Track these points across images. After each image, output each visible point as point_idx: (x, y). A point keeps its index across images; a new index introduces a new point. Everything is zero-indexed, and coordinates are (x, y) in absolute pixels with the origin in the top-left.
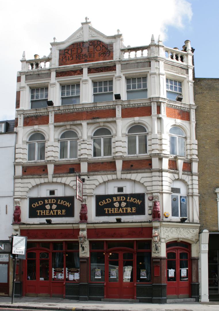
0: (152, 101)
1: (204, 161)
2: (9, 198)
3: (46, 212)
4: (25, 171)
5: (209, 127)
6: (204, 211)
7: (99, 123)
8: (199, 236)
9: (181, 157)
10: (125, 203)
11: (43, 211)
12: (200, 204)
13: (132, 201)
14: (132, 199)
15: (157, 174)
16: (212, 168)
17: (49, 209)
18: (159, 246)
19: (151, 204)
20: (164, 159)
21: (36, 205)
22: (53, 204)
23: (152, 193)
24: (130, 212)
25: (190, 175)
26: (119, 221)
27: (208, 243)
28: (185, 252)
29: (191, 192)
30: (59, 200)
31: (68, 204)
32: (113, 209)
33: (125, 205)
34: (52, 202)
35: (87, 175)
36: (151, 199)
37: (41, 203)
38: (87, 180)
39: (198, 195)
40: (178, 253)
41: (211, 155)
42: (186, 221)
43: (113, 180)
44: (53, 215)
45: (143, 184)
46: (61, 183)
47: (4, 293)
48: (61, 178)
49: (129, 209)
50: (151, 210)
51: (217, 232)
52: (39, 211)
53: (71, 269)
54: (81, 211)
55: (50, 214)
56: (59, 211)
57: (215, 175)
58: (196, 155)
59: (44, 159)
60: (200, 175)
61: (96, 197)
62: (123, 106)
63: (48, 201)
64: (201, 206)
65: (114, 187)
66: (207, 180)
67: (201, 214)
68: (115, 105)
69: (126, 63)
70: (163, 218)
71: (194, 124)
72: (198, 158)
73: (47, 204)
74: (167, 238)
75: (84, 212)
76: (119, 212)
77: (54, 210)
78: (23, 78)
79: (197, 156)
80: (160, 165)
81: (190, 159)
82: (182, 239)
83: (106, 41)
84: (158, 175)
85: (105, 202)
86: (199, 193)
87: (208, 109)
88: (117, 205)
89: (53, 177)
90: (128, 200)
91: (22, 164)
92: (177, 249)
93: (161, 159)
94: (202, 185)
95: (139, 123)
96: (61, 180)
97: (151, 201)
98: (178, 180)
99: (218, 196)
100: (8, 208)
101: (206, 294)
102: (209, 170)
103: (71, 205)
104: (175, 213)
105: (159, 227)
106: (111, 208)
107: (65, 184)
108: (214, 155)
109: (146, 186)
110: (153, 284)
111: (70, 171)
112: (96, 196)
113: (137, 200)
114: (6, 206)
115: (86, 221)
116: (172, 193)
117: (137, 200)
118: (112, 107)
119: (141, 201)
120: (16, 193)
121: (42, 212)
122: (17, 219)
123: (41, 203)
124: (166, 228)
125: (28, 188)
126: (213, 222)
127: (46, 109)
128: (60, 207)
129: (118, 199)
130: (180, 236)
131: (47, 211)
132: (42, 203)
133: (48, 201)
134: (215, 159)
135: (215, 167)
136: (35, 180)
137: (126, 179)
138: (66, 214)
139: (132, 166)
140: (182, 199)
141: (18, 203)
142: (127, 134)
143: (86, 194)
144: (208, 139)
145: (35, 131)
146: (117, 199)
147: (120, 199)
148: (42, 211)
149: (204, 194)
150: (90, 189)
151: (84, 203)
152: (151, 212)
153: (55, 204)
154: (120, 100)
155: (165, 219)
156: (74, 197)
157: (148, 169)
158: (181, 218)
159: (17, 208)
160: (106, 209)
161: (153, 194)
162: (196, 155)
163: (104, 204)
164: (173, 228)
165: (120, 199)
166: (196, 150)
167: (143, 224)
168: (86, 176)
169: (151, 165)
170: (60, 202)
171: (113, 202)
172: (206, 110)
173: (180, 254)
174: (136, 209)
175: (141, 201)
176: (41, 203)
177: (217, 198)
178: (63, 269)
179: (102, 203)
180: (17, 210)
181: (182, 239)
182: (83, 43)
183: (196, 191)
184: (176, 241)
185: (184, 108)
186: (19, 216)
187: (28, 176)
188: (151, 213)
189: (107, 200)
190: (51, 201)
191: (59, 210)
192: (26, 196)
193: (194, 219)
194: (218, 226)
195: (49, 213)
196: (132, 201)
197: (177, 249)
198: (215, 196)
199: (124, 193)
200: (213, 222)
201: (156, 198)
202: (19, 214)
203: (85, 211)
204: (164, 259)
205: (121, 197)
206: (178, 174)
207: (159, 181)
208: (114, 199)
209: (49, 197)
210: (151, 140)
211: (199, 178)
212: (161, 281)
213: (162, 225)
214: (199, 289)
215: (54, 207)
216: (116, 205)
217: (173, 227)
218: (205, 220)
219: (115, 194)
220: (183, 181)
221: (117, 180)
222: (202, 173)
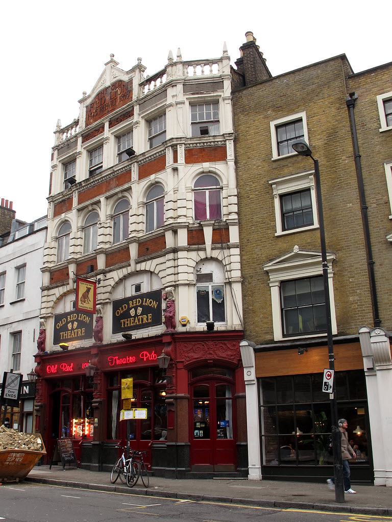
0: (166, 146)
5: (255, 163)
6: (251, 307)
7: (116, 194)
15: (171, 256)
20: (179, 231)
35: (104, 274)
43: (130, 275)
60: (241, 246)
62: (140, 163)
67: (247, 312)
68: (131, 164)
69: (143, 101)
71: (232, 164)
78: (56, 152)
83: (125, 78)
87: (253, 134)
91: (75, 260)
93: (175, 232)
95: (210, 172)
98: (207, 260)
101: (255, 465)
106: (65, 331)
107: (152, 273)
118: (219, 143)
122: (41, 344)
123: (125, 306)
125: (110, 286)
126: (266, 326)
127: (75, 186)
128: (147, 310)
130: (208, 357)
139: (148, 249)
140: (218, 292)
142: (193, 188)
143: (102, 301)
144: (253, 183)
145: (203, 172)
149: (250, 276)
151: (99, 316)
154: (207, 135)
163: (151, 306)
172: (249, 135)
180: (43, 332)
182: (106, 89)
183: (237, 274)
185: (202, 144)
187: (153, 255)
192: (109, 299)
198: (265, 278)
200: (266, 326)
206: (205, 250)
210: (177, 201)
215: (140, 310)
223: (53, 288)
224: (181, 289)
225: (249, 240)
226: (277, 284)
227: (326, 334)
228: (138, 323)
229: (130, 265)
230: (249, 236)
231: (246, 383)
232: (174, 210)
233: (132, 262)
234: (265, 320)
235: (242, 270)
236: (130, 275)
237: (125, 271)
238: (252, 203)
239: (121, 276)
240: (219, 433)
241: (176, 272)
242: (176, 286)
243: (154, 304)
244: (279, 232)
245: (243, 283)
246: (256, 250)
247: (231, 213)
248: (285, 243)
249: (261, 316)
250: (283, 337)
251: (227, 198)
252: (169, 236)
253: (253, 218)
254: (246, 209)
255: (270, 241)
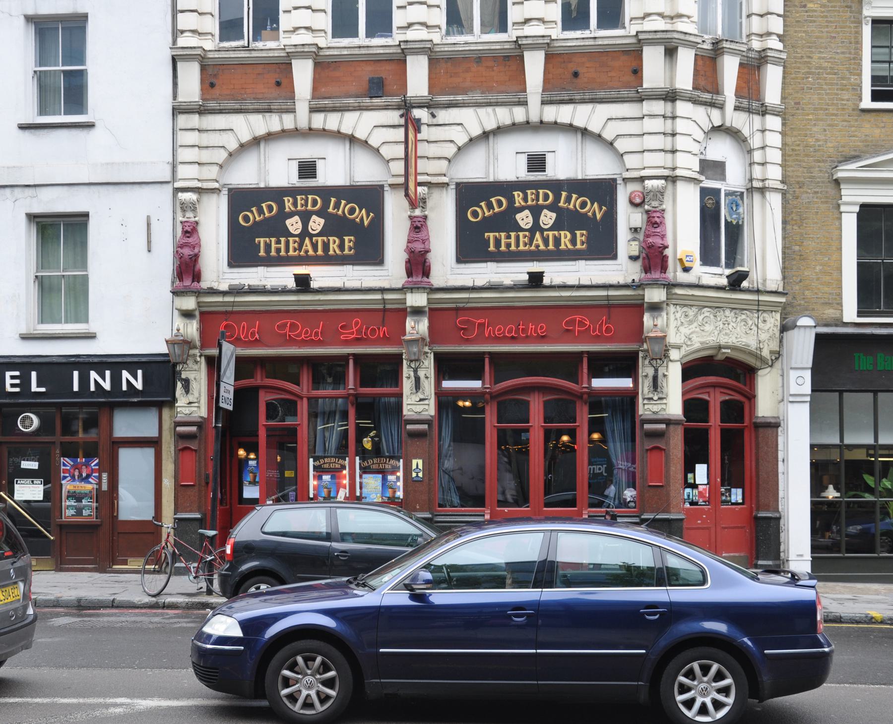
1: (802, 57)
2: (66, 188)
3: (287, 243)
4: (212, 85)
6: (797, 248)
8: (781, 341)
9: (733, 46)
10: (554, 215)
11: (278, 242)
12: (784, 222)
13: (575, 206)
14: (578, 199)
15: (658, 107)
16: (824, 87)
17: (298, 232)
18: (665, 376)
19: (637, 218)
21: (483, 211)
22: (542, 207)
23: (642, 179)
24: (570, 246)
25: (759, 114)
26: (303, 282)
27: (810, 365)
28: (737, 397)
29: (760, 177)
30: (333, 200)
31: (362, 216)
32: (513, 234)
33: (551, 222)
34: (309, 207)
36: (638, 200)
37: (270, 210)
38: (428, 125)
39: (781, 186)
40: (715, 400)
41: (825, 35)
42: (745, 284)
43: (514, 128)
44: (311, 257)
45: (611, 144)
46: (339, 132)
47: (142, 561)
48: (339, 114)
49: (565, 237)
50: (637, 243)
51: (836, 325)
52: (262, 240)
53: (370, 461)
54: (409, 242)
55: (302, 253)
56: (335, 242)
57: (836, 115)
58: (778, 36)
59: (277, 39)
61: (456, 189)
63: (295, 204)
64: (788, 227)
65: (517, 153)
66: (808, 132)
70: (675, 271)
72: (785, 47)
73: (521, 209)
74: (687, 345)
75: (419, 247)
76: (533, 248)
77: (314, 239)
79: (781, 38)
80: (668, 74)
81: (759, 52)
82: (729, 351)
84: (663, 113)
85: (485, 210)
86: (782, 182)
88: (526, 220)
89: (313, 110)
90: (561, 204)
92: (714, 386)
93: (671, 52)
94: (793, 150)
96: (340, 122)
97: (639, 210)
99: (843, 192)
100: (153, 227)
101: (802, 556)
102: (819, 94)
103: (373, 219)
104: (708, 256)
105: (665, 306)
107: (352, 139)
108: (835, 37)
109: (622, 151)
110: (643, 517)
111: (370, 89)
112: (458, 184)
113: (592, 204)
114: (148, 218)
115: (425, 279)
116: (701, 181)
117: (592, 204)
119: (604, 208)
120: (184, 171)
121: (273, 246)
123: (270, 208)
124: (685, 309)
126: (826, 289)
129: (529, 197)
130: (723, 340)
131: (291, 239)
132: (504, 205)
133: (295, 204)
134: (837, 53)
135: (837, 84)
136: (247, 120)
137: (556, 123)
138: (356, 253)
140: (736, 197)
141: (192, 207)
146: (525, 199)
147: (538, 200)
148: (273, 240)
149: (798, 183)
150: (439, 158)
152: (637, 247)
153: (319, 214)
155: (682, 277)
156: (382, 186)
157: (627, 86)
158: (728, 272)
159: (187, 228)
160: (491, 235)
161: (647, 182)
162: (778, 36)
163: (484, 218)
164: (706, 309)
165: (538, 199)
166: (779, 15)
167: (612, 293)
168: (426, 109)
169: (637, 72)
170: (337, 206)
171: (513, 210)
173: (724, 403)
174: (588, 238)
175: (604, 208)
176: (270, 208)
177: (840, 202)
178: (347, 462)
179: (476, 211)
181: (729, 351)
183: (774, 173)
184: (709, 359)
186: (195, 258)
187: (601, 94)
188: (636, 253)
189: (493, 200)
190: (307, 201)
191: (331, 239)
193: (768, 277)
194: (841, 304)
195: (300, 249)
196: (575, 206)
197: (714, 386)
198: (832, 191)
199: (548, 178)
200: (826, 289)
201: (655, 198)
202: (196, 251)
203: (424, 242)
204: (677, 422)
205: (541, 191)
206: (721, 107)
207: (664, 134)
208: (516, 196)
209: (298, 185)
211: (783, 124)
212: (669, 505)
213: (674, 296)
214: (782, 535)
216: (524, 219)
217: (702, 304)
218: (800, 281)
219: (520, 179)
220: (734, 134)
221: (296, 134)
222: (796, 103)
223: (221, 112)
224: (680, 185)
225: (798, 103)
226: (857, 209)
227: (76, 374)
228: (542, 247)
229: (293, 111)
230: (799, 95)
231: (808, 399)
232: (762, 16)
233: (302, 108)
234: (827, 278)
235: (783, 166)
236: (514, 128)
237: (274, 123)
238: (811, 22)
239: (491, 125)
240: (723, 494)
241: (669, 148)
242: (672, 179)
243: (595, 210)
244: (867, 103)
245: (784, 194)
246: (815, 129)
247: (649, 15)
248: (878, 127)
249: (818, 268)
250: (858, 316)
251: (404, 7)
252: (652, 59)
253: (810, 57)
254: (796, 32)
255: (847, 117)
